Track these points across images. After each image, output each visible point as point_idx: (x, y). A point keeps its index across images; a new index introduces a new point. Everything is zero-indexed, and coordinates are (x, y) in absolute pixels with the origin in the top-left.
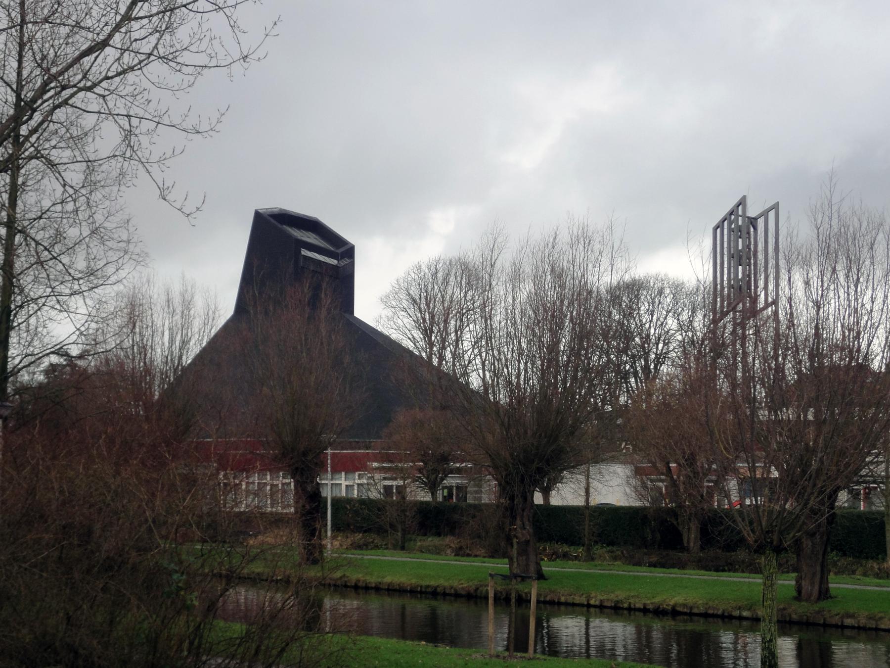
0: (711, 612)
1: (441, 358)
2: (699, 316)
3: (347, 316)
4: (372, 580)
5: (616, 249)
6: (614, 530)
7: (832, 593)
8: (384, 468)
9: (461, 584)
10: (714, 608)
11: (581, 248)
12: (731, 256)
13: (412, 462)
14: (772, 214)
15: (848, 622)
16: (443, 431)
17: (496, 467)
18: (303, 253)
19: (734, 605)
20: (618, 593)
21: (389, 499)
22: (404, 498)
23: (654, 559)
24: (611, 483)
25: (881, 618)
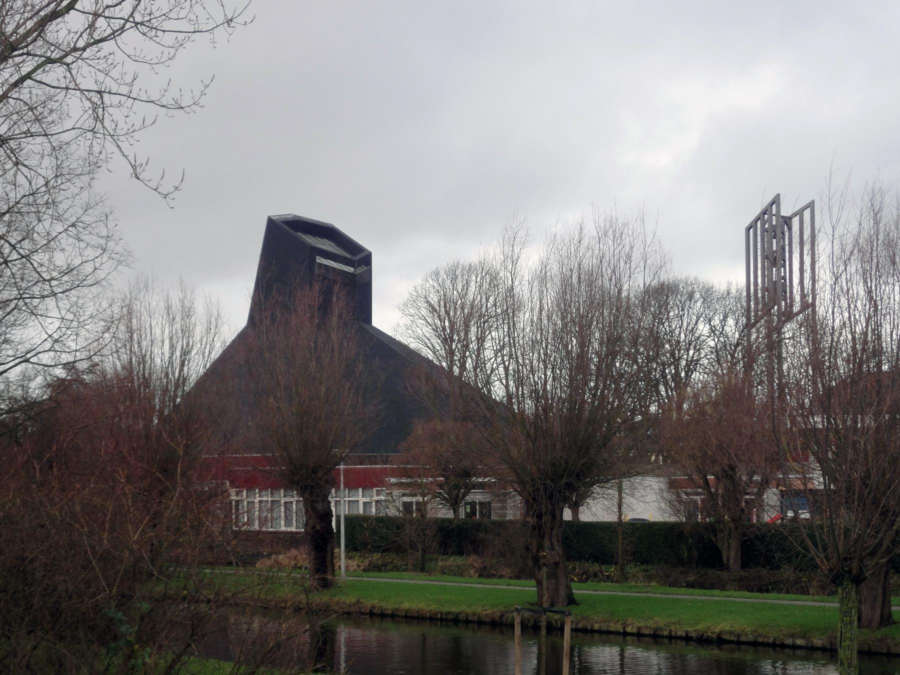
0: (760, 640)
1: (463, 367)
2: (731, 322)
3: (365, 326)
4: (389, 606)
5: (648, 242)
6: (649, 547)
7: (895, 617)
8: (402, 483)
9: (484, 609)
10: (765, 636)
11: (611, 243)
12: (765, 257)
14: (798, 217)
16: (464, 444)
17: (521, 482)
18: (318, 261)
20: (657, 619)
22: (423, 516)
23: (691, 578)
24: (647, 499)
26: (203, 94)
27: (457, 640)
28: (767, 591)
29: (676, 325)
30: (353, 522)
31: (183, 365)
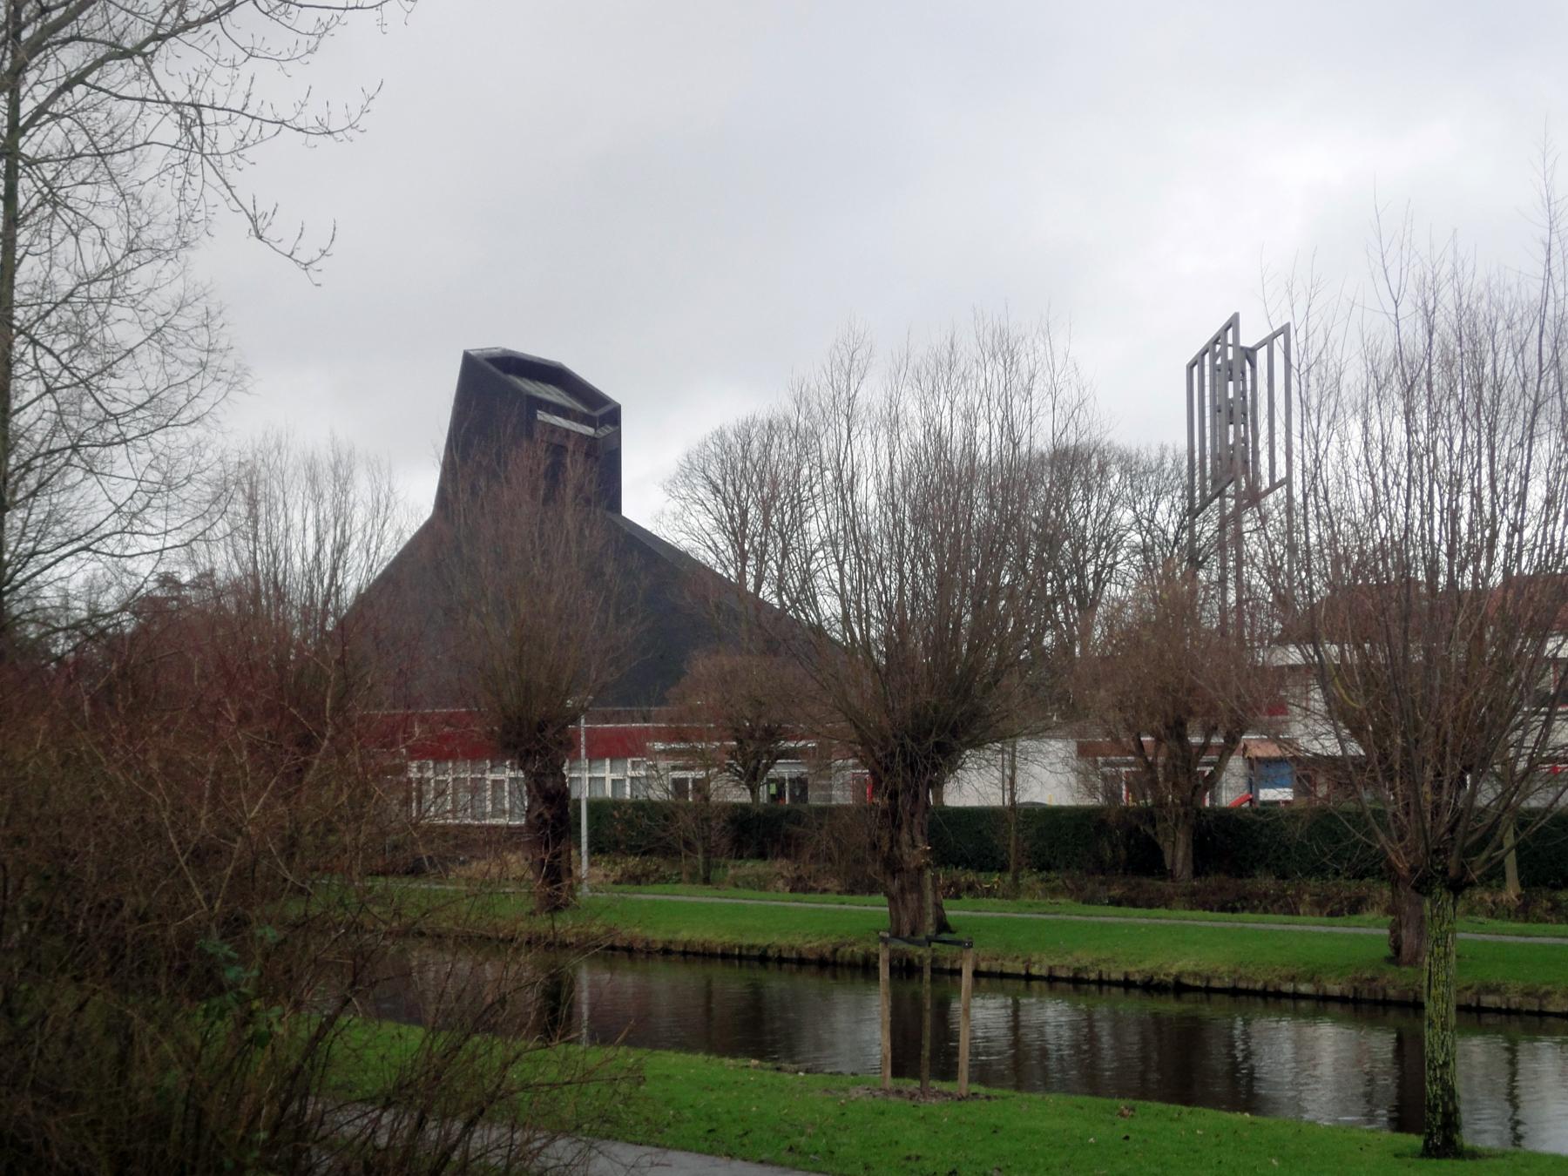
0: (1243, 985)
3: (609, 515)
4: (659, 936)
6: (1062, 849)
9: (810, 942)
10: (1249, 979)
11: (1001, 369)
12: (1216, 410)
13: (720, 739)
14: (1281, 338)
15: (1489, 1000)
17: (865, 742)
19: (1284, 972)
20: (1078, 954)
21: (681, 801)
22: (707, 799)
23: (1116, 892)
25: (1548, 994)
26: (364, 110)
27: (757, 992)
28: (1234, 910)
29: (1083, 511)
30: (596, 808)
31: (334, 569)
